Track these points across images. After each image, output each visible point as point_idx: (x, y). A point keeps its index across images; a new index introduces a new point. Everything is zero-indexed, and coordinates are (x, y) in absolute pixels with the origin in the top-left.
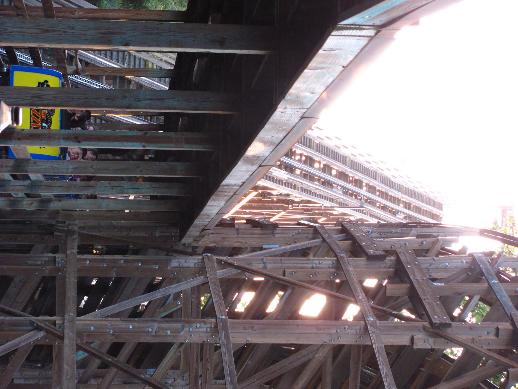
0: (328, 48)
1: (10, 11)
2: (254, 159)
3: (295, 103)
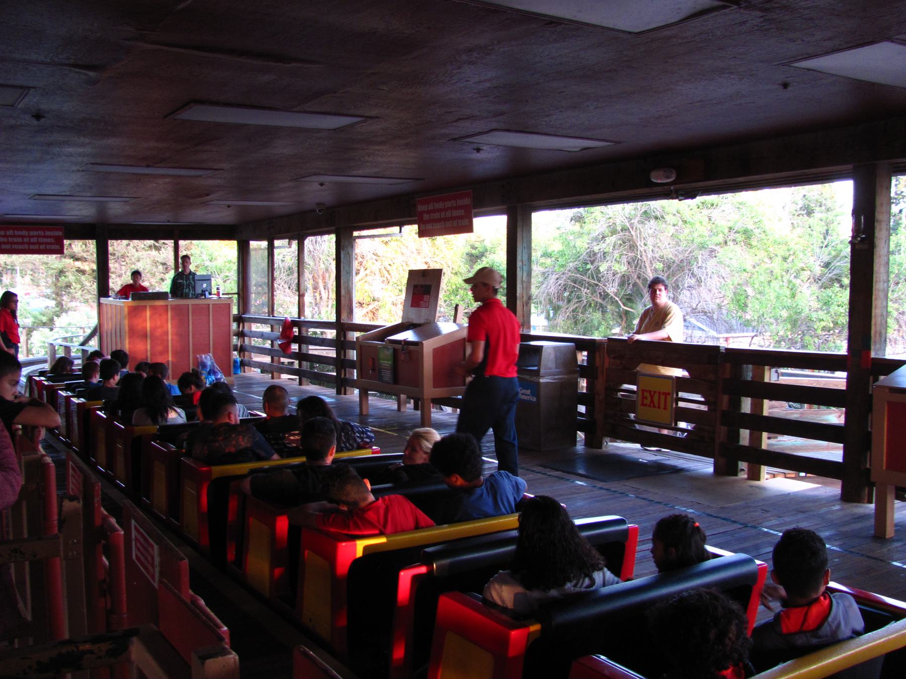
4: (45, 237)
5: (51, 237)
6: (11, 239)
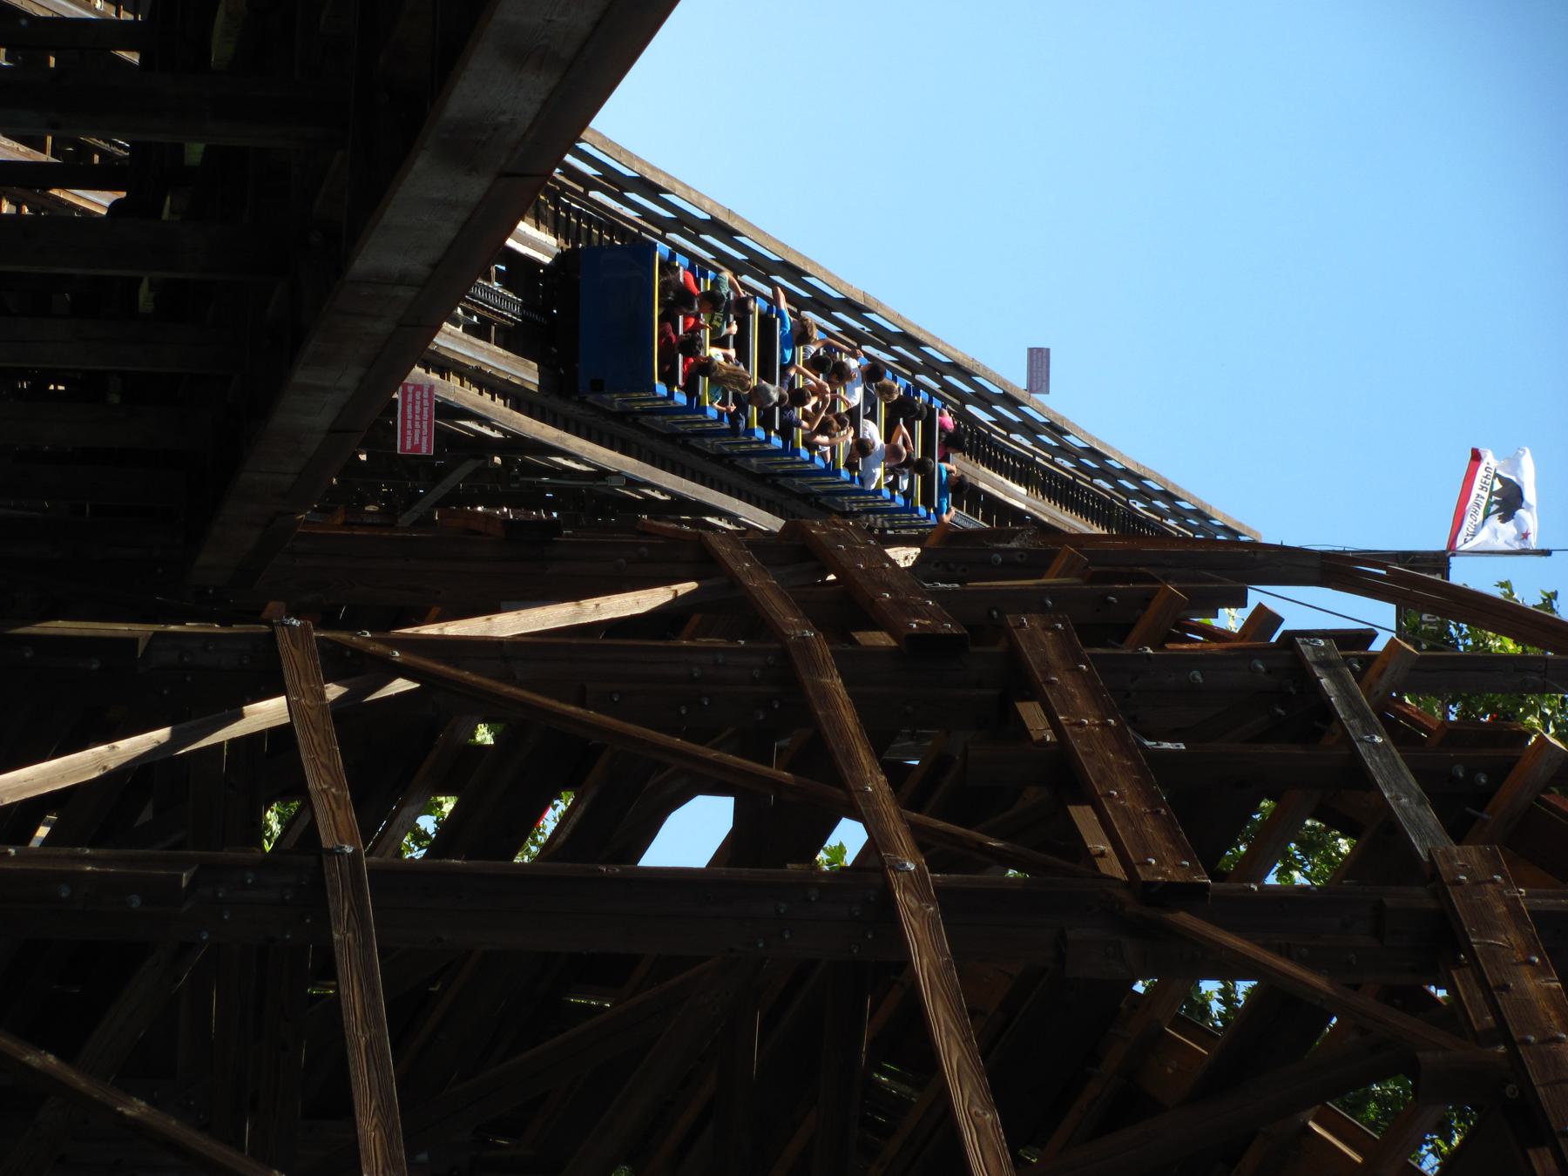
4: (421, 436)
5: (420, 441)
6: (418, 403)
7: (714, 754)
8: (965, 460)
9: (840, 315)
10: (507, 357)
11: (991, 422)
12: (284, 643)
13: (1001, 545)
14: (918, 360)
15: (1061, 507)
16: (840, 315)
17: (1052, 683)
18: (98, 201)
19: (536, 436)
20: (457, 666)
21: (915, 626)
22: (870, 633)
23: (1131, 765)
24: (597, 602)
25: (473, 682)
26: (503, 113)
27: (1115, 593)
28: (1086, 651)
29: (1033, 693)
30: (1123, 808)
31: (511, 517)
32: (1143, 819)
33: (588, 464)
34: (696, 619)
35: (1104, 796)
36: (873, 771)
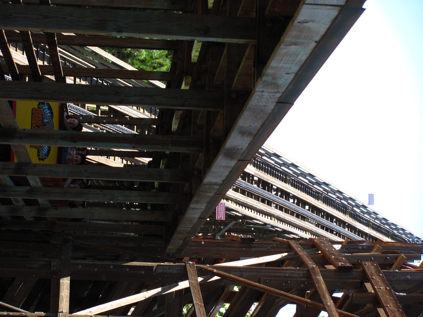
0: (302, 19)
1: (16, 37)
2: (234, 153)
3: (271, 85)
7: (291, 295)
8: (353, 221)
9: (323, 186)
10: (243, 196)
11: (360, 212)
12: (188, 267)
13: (361, 244)
14: (342, 197)
15: (377, 232)
16: (323, 186)
17: (373, 278)
18: (146, 160)
19: (249, 215)
20: (229, 273)
21: (340, 264)
22: (329, 265)
23: (393, 299)
24: (263, 258)
25: (233, 277)
26: (239, 146)
27: (389, 256)
28: (382, 271)
29: (369, 281)
30: (391, 310)
31: (243, 237)
32: (396, 312)
33: (262, 222)
34: (287, 262)
35: (386, 306)
36: (330, 300)
